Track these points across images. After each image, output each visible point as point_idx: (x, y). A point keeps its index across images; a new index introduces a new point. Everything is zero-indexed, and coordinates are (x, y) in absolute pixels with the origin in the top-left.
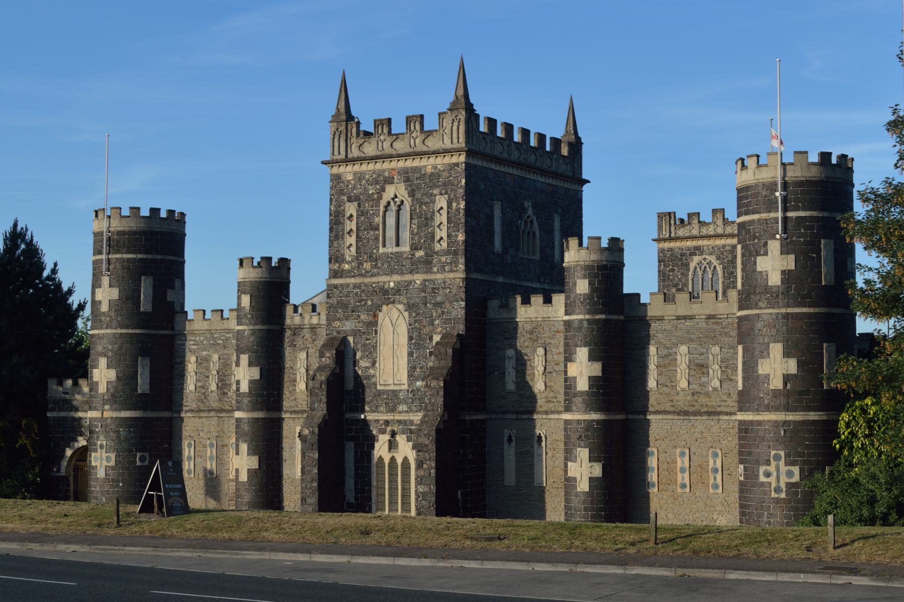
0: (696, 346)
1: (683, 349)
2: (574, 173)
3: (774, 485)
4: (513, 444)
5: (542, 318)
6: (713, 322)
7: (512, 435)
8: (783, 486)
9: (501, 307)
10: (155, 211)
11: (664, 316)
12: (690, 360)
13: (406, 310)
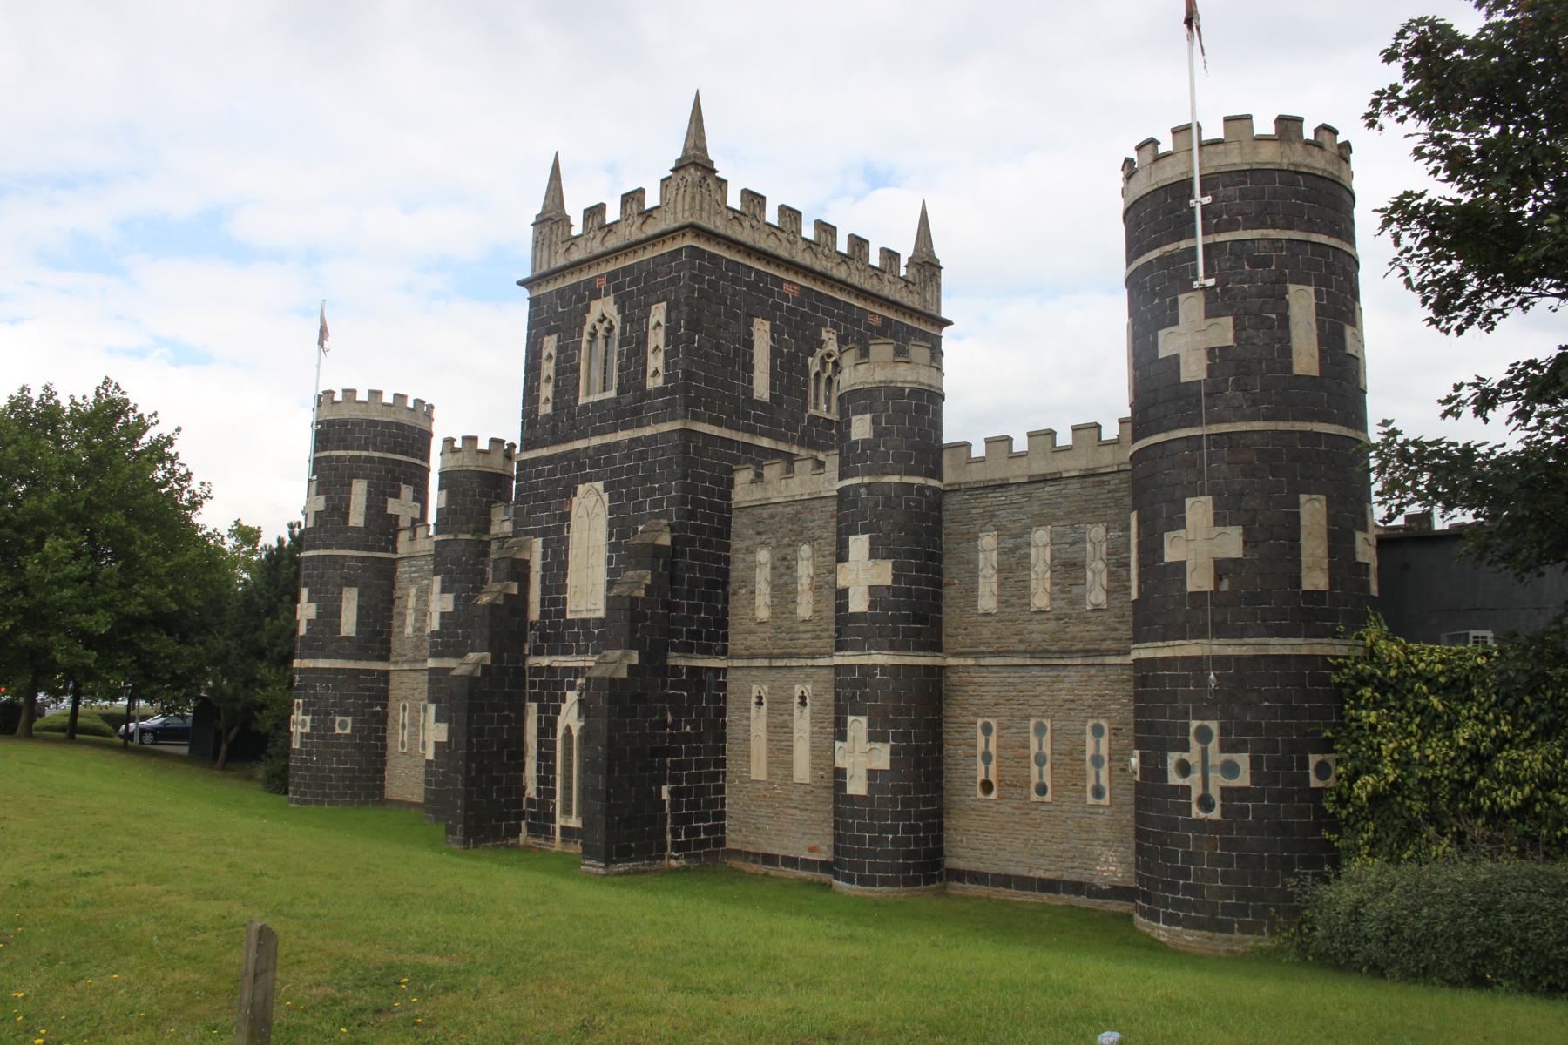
1: (1041, 536)
2: (925, 307)
3: (1196, 793)
5: (810, 494)
6: (1093, 482)
7: (762, 694)
8: (1215, 793)
9: (752, 482)
11: (1008, 479)
12: (1052, 555)
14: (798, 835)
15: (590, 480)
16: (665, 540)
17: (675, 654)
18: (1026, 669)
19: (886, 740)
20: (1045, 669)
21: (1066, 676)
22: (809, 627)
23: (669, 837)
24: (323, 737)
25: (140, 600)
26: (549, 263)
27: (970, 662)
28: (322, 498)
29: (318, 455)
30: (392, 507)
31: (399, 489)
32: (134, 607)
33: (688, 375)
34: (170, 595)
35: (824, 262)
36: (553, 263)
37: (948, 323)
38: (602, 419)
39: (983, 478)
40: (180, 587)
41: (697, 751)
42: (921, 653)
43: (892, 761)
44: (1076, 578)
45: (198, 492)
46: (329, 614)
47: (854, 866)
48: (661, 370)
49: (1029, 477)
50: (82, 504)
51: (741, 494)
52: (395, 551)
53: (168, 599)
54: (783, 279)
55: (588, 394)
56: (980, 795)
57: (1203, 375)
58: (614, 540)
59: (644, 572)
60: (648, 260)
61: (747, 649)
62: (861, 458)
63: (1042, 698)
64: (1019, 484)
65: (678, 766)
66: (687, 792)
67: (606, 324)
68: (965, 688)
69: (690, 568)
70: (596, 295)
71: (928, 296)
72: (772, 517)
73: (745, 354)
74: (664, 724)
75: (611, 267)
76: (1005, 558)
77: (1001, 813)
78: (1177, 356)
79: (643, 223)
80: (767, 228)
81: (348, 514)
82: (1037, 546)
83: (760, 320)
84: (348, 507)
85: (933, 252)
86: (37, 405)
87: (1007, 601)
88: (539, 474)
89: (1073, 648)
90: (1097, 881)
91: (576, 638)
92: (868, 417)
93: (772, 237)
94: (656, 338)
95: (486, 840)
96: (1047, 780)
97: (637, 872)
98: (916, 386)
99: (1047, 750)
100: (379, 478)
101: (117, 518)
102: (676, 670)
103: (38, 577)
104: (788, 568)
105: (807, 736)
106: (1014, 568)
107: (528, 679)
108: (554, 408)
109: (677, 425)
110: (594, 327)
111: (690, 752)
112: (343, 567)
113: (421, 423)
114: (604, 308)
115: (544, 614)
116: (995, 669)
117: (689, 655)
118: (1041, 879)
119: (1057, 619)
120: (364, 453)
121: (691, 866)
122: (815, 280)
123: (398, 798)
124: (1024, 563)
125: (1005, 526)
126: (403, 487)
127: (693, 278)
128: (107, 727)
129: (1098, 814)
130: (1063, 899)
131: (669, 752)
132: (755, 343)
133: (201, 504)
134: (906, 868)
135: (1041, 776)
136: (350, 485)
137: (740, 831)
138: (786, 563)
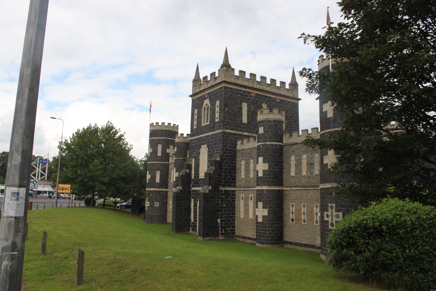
0: (309, 155)
3: (330, 222)
4: (243, 200)
9: (241, 144)
10: (169, 124)
11: (297, 142)
13: (207, 147)
14: (250, 232)
15: (204, 144)
16: (218, 159)
17: (221, 187)
18: (301, 190)
19: (267, 208)
20: (305, 190)
21: (310, 192)
22: (253, 180)
23: (220, 232)
24: (152, 207)
25: (116, 174)
26: (196, 91)
27: (289, 189)
28: (151, 149)
29: (150, 139)
30: (168, 151)
31: (170, 146)
32: (114, 176)
33: (224, 118)
34: (123, 173)
35: (263, 87)
36: (197, 91)
37: (300, 99)
38: (206, 129)
39: (292, 142)
40: (126, 171)
41: (227, 211)
42: (276, 186)
43: (268, 213)
44: (312, 167)
45: (129, 147)
46: (153, 178)
47: (260, 240)
48: (218, 117)
49: (302, 141)
50: (102, 151)
51: (239, 147)
52: (169, 162)
53: (122, 174)
54: (251, 92)
55: (204, 123)
56: (291, 222)
57: (332, 116)
58: (209, 159)
59: (213, 167)
60: (216, 90)
61: (240, 185)
62: (261, 138)
63: (305, 198)
64: (300, 143)
65: (222, 214)
66: (225, 221)
67: (207, 106)
68: (288, 195)
69: (225, 166)
70: (205, 99)
71: (294, 93)
72: (245, 152)
73: (240, 112)
74: (218, 204)
75: (208, 92)
76: (297, 162)
77: (296, 227)
78: (327, 111)
79: (215, 80)
80: (246, 79)
81: (157, 153)
82: (304, 159)
83: (244, 103)
84: (157, 151)
85: (296, 81)
86: (93, 128)
87: (297, 173)
88: (194, 143)
89: (312, 185)
90: (317, 245)
91: (201, 183)
92: (262, 128)
93: (248, 82)
94: (217, 109)
95: (181, 232)
96: (306, 219)
97: (211, 240)
98: (274, 119)
99: (306, 211)
100: (164, 144)
101: (111, 154)
102: (222, 191)
103: (92, 169)
104: (248, 165)
105: (252, 207)
106: (298, 165)
107: (192, 193)
108: (197, 127)
109: (221, 131)
110: (205, 107)
111: (225, 211)
112: (156, 166)
113: (175, 130)
114: (207, 102)
115: (195, 177)
116: (294, 190)
117: (225, 187)
118: (304, 244)
119: (308, 178)
120: (161, 138)
121: (226, 239)
122: (260, 91)
123: (170, 222)
124: (301, 164)
125: (297, 154)
126: (171, 146)
127: (225, 94)
128: (114, 205)
129: (317, 227)
130: (309, 249)
131: (220, 211)
132: (243, 109)
133: (131, 150)
134: (272, 240)
135: (304, 218)
136: (158, 146)
137: (238, 230)
138: (248, 164)
